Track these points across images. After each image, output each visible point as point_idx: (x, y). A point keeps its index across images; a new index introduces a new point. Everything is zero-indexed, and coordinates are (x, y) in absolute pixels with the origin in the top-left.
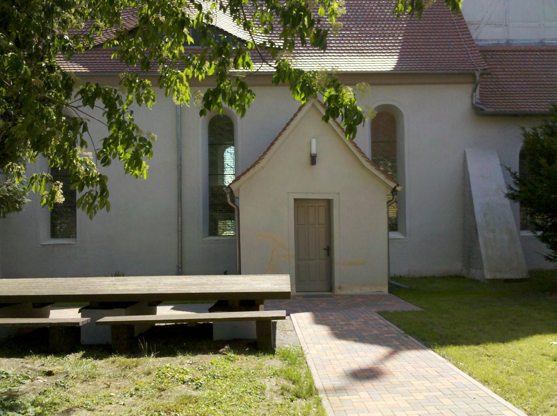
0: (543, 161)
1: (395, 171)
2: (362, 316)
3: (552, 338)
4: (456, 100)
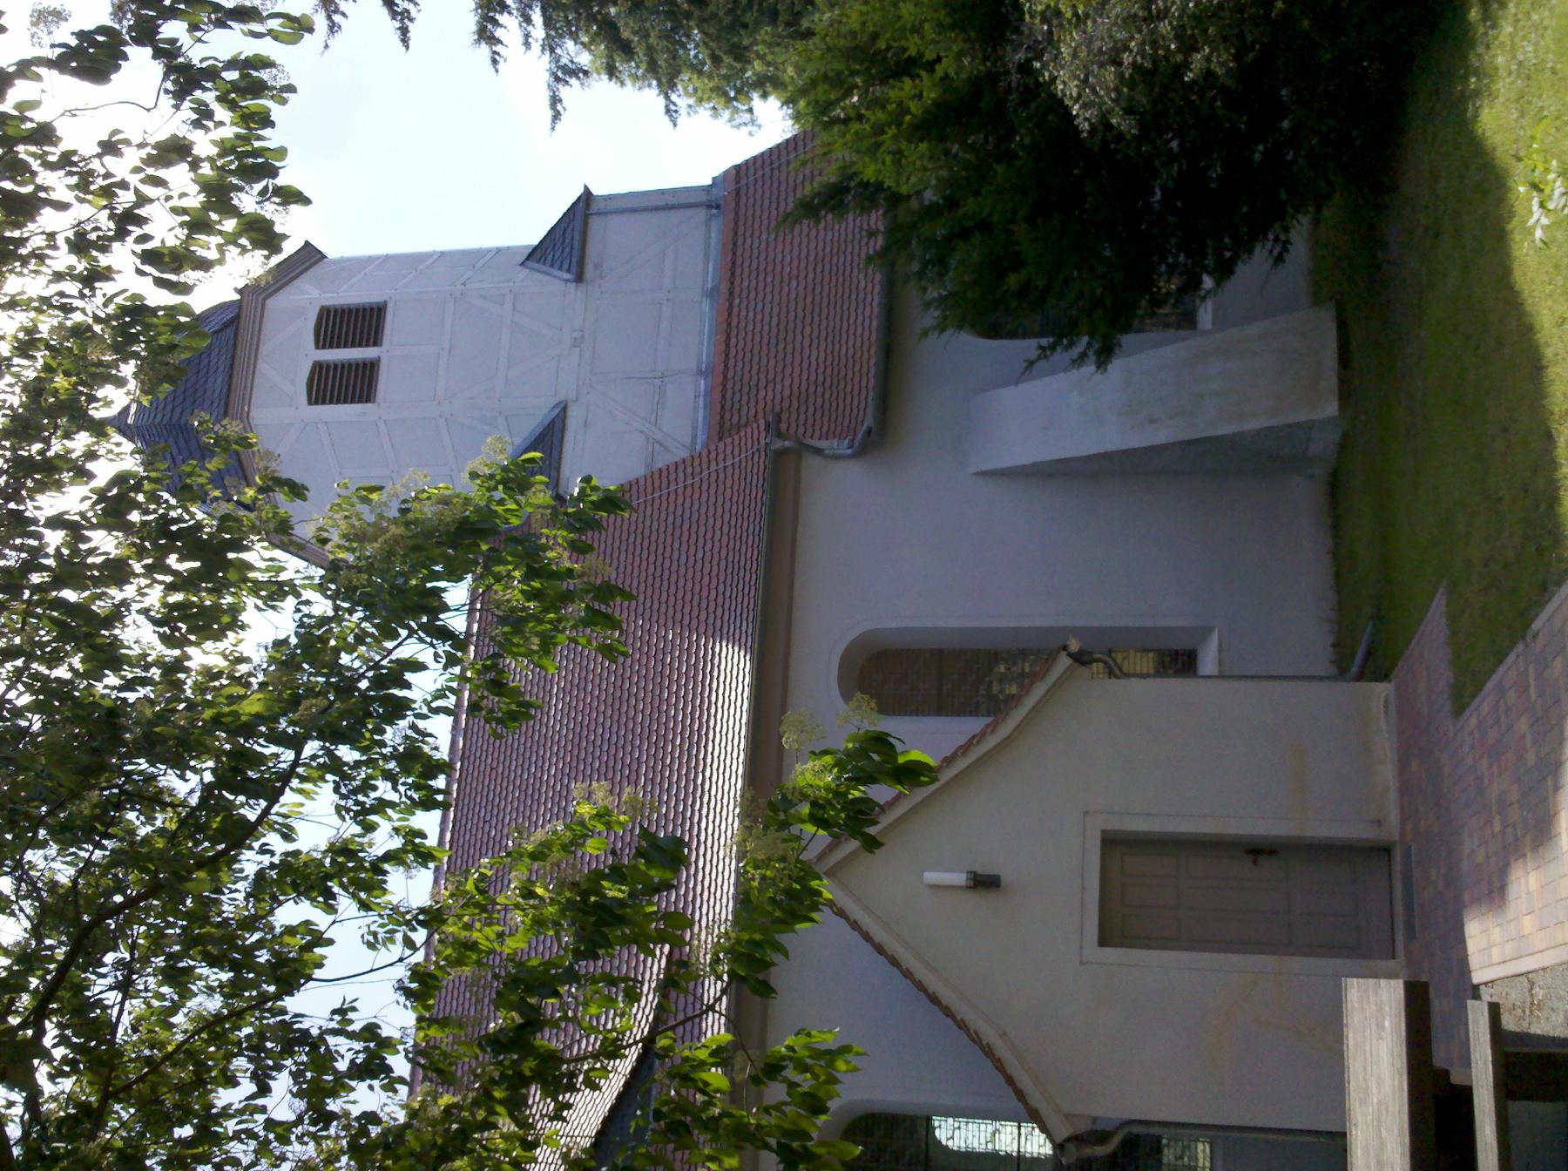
0: (1013, 281)
1: (1023, 654)
2: (1469, 762)
3: (1522, 241)
4: (839, 494)
